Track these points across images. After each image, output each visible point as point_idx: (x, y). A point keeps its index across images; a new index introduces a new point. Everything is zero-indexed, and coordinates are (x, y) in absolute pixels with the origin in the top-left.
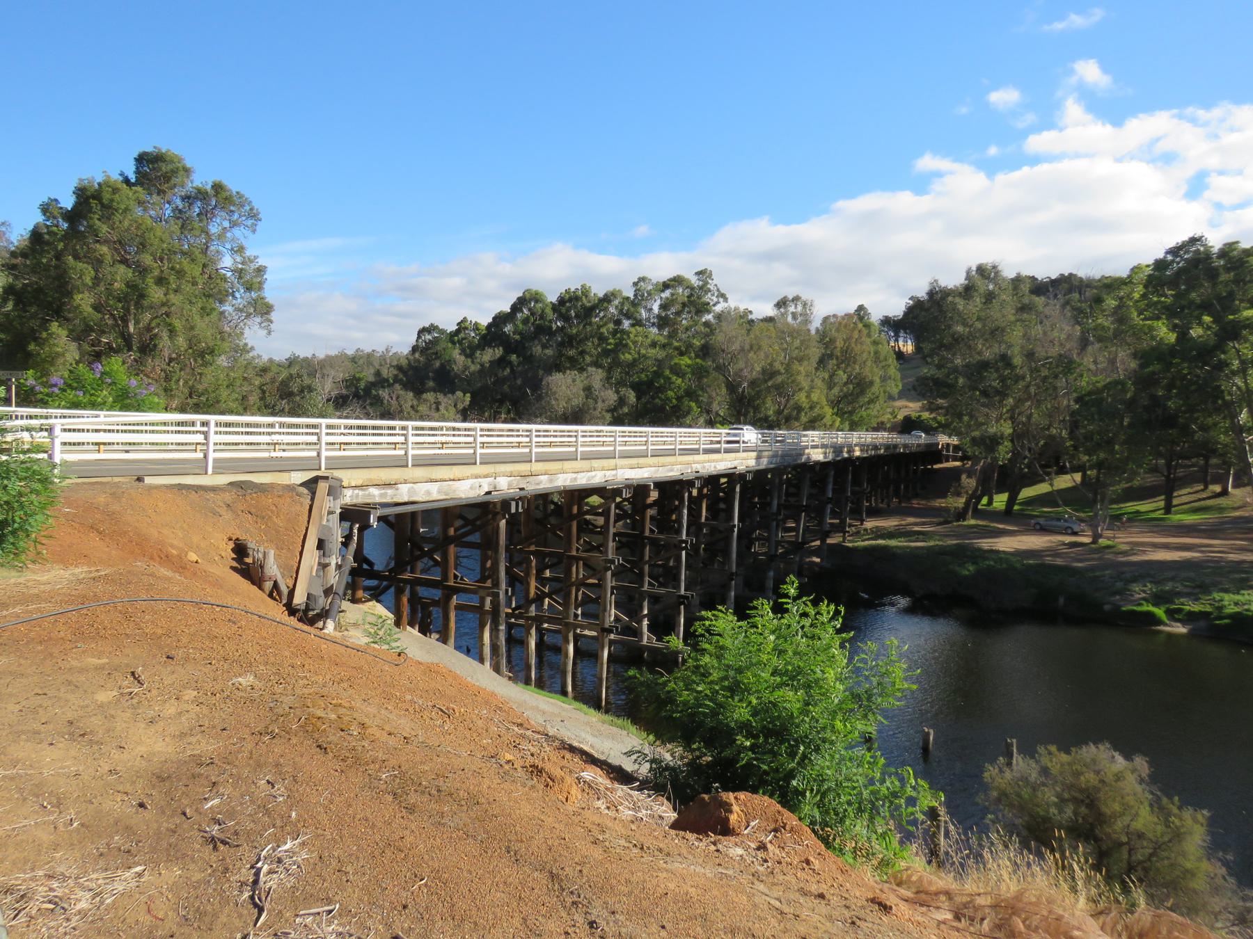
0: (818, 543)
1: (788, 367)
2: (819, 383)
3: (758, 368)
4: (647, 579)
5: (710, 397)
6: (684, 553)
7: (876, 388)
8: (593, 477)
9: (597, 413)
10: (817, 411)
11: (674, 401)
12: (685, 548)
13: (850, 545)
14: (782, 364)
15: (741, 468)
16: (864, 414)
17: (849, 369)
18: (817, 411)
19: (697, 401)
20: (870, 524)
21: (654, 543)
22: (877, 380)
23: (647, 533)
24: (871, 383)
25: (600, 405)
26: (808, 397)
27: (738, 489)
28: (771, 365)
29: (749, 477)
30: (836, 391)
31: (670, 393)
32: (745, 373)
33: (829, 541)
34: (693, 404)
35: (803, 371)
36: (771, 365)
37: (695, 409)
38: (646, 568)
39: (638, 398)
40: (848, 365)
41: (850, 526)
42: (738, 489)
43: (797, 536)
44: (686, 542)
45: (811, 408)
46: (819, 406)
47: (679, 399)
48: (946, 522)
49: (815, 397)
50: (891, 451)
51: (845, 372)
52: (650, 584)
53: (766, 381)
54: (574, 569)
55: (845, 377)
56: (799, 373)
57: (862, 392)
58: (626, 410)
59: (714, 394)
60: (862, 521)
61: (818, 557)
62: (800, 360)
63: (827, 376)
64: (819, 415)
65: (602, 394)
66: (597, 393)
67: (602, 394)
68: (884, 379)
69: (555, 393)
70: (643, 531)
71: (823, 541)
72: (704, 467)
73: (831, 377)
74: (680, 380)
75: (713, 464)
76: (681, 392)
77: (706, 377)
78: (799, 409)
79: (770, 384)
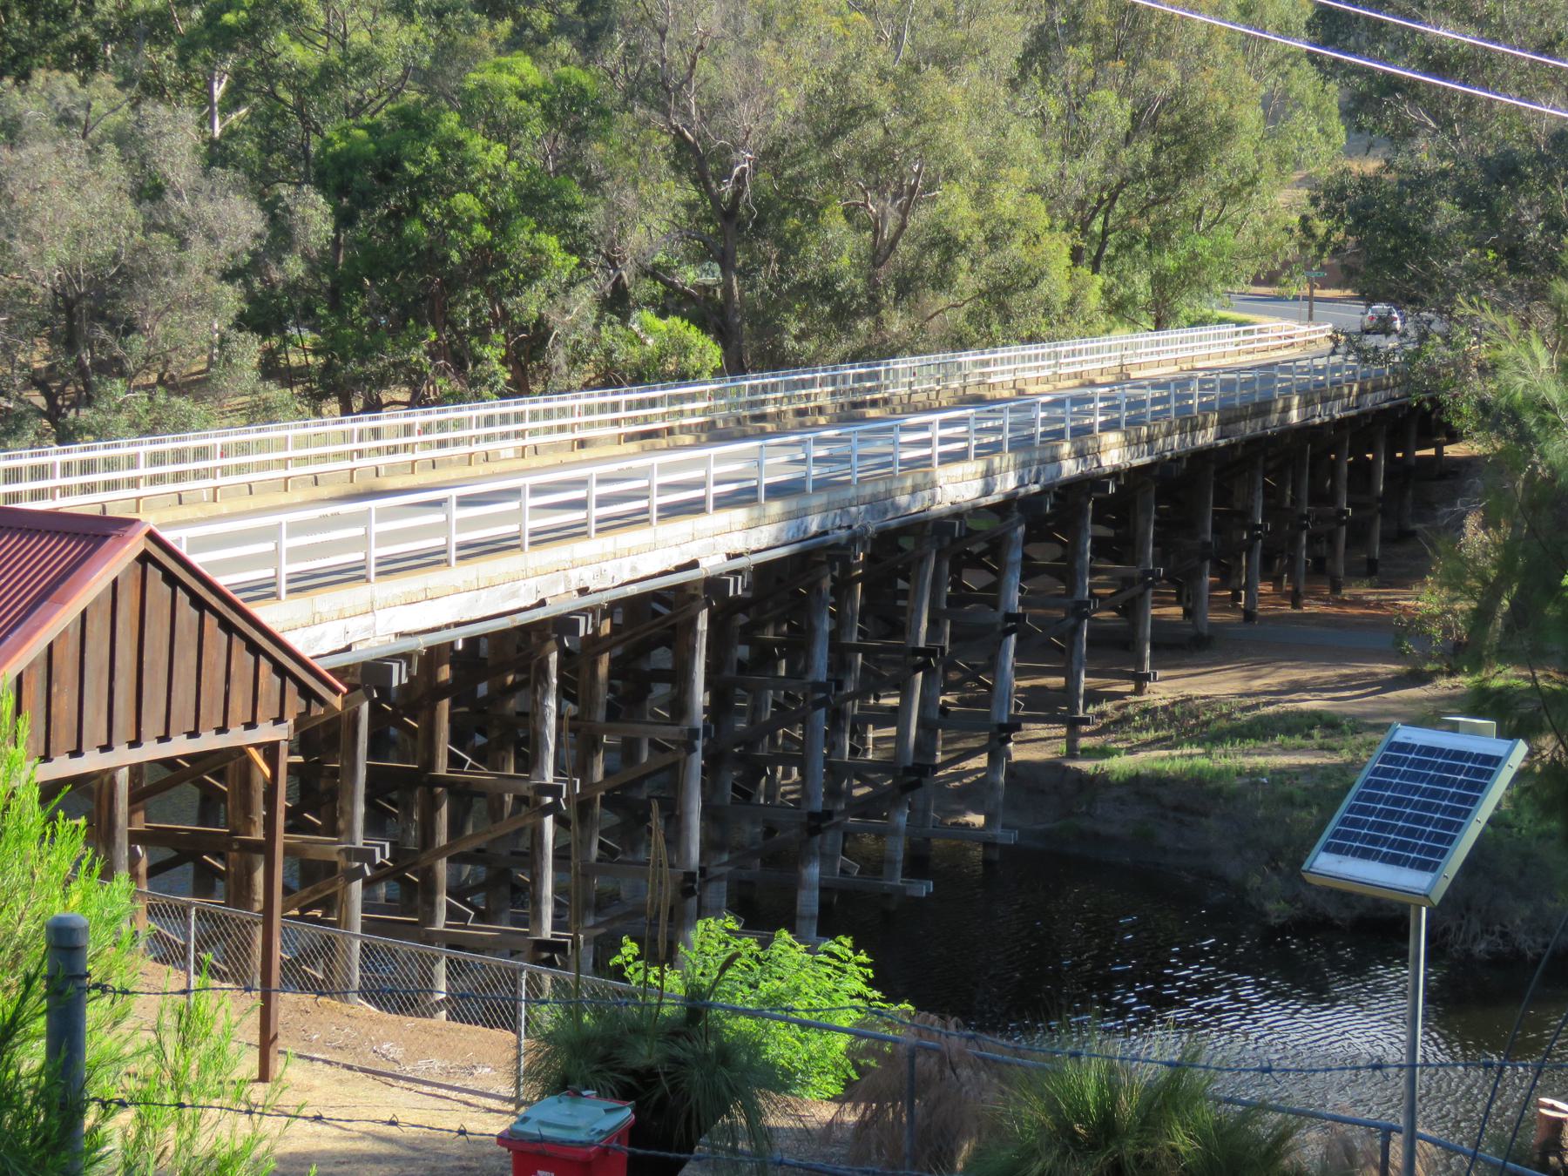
0: (981, 761)
1: (904, 84)
2: (1025, 140)
3: (790, 103)
4: (443, 899)
5: (612, 208)
6: (549, 821)
7: (1241, 150)
8: (318, 640)
9: (180, 285)
10: (1016, 249)
11: (479, 230)
12: (554, 808)
13: (1087, 766)
14: (883, 75)
15: (713, 563)
16: (1203, 244)
17: (1141, 79)
18: (1016, 249)
19: (562, 228)
20: (1163, 690)
21: (463, 795)
22: (1250, 117)
23: (442, 768)
24: (1228, 129)
25: (199, 249)
26: (981, 198)
27: (702, 624)
28: (840, 79)
29: (737, 589)
30: (1091, 165)
31: (464, 201)
32: (744, 115)
33: (1019, 753)
34: (550, 243)
35: (958, 102)
36: (840, 79)
37: (559, 257)
38: (442, 866)
39: (344, 219)
40: (1136, 63)
41: (1094, 697)
42: (702, 624)
43: (901, 737)
44: (554, 790)
45: (993, 241)
46: (1020, 236)
47: (498, 219)
48: (1417, 678)
49: (1006, 201)
50: (1248, 428)
51: (1123, 93)
52: (452, 913)
53: (826, 141)
54: (259, 876)
55: (1121, 116)
56: (946, 111)
57: (1192, 165)
58: (294, 267)
59: (629, 201)
60: (1140, 680)
61: (977, 812)
62: (946, 60)
63: (1054, 107)
64: (1022, 270)
65: (207, 209)
66: (185, 205)
67: (207, 209)
68: (1276, 110)
69: (29, 213)
70: (430, 763)
71: (996, 750)
72: (602, 573)
73: (1072, 111)
74: (500, 150)
75: (626, 563)
76: (507, 197)
77: (601, 135)
78: (948, 245)
79: (839, 149)
